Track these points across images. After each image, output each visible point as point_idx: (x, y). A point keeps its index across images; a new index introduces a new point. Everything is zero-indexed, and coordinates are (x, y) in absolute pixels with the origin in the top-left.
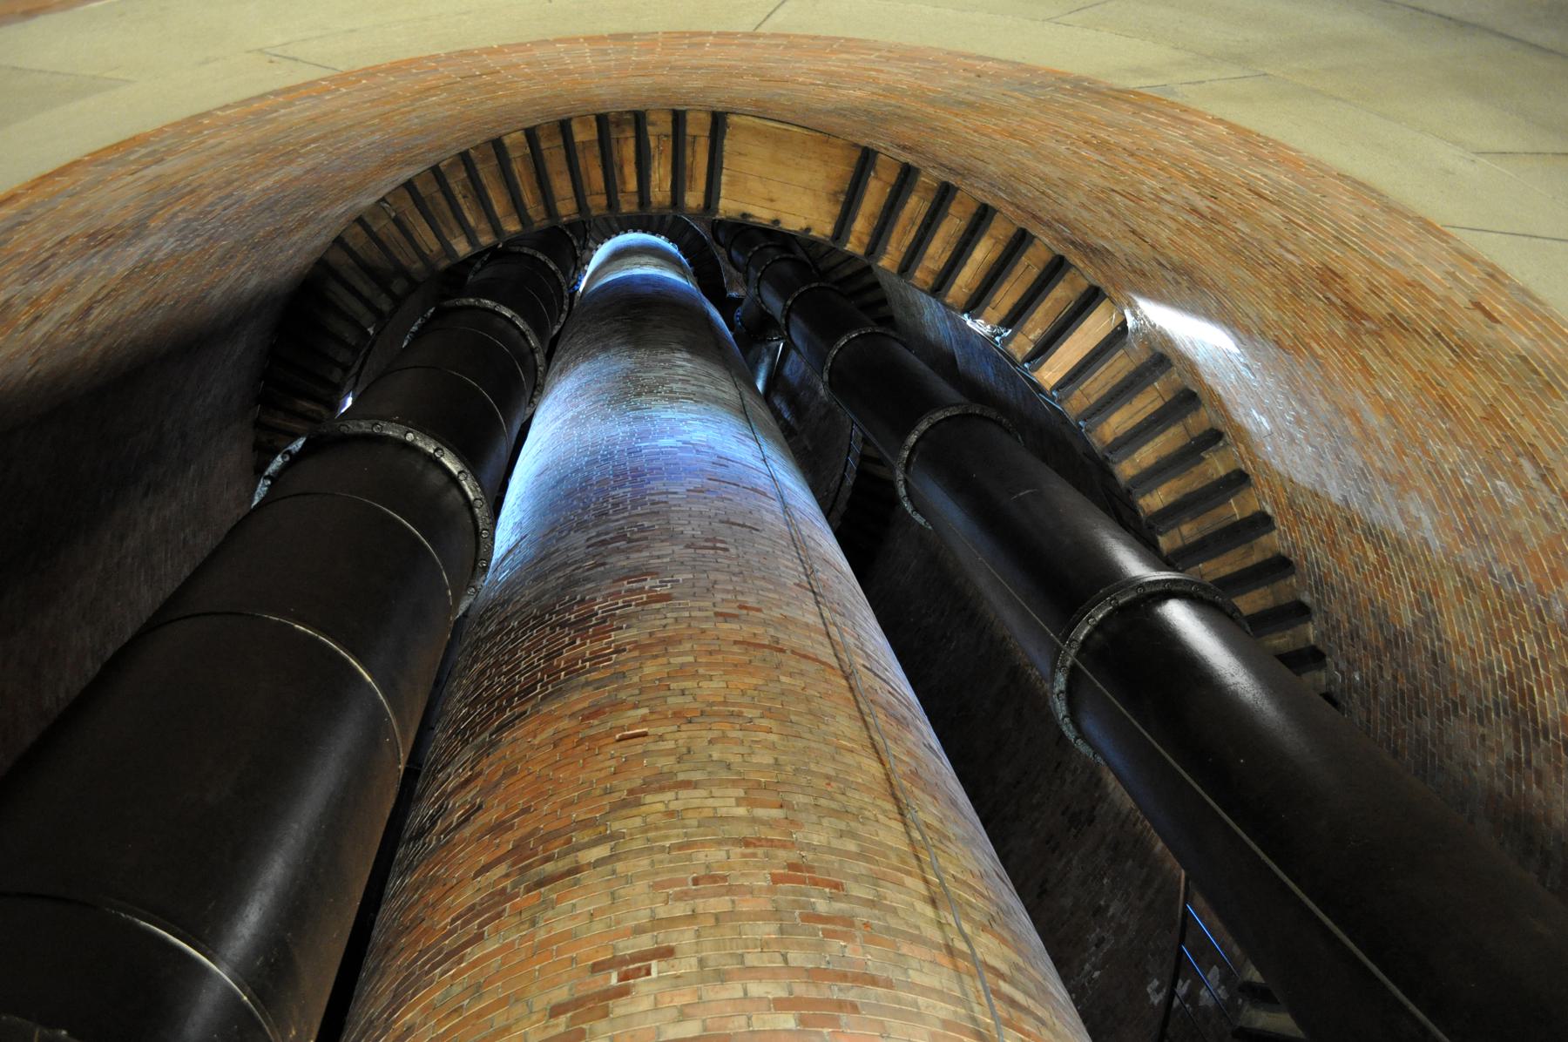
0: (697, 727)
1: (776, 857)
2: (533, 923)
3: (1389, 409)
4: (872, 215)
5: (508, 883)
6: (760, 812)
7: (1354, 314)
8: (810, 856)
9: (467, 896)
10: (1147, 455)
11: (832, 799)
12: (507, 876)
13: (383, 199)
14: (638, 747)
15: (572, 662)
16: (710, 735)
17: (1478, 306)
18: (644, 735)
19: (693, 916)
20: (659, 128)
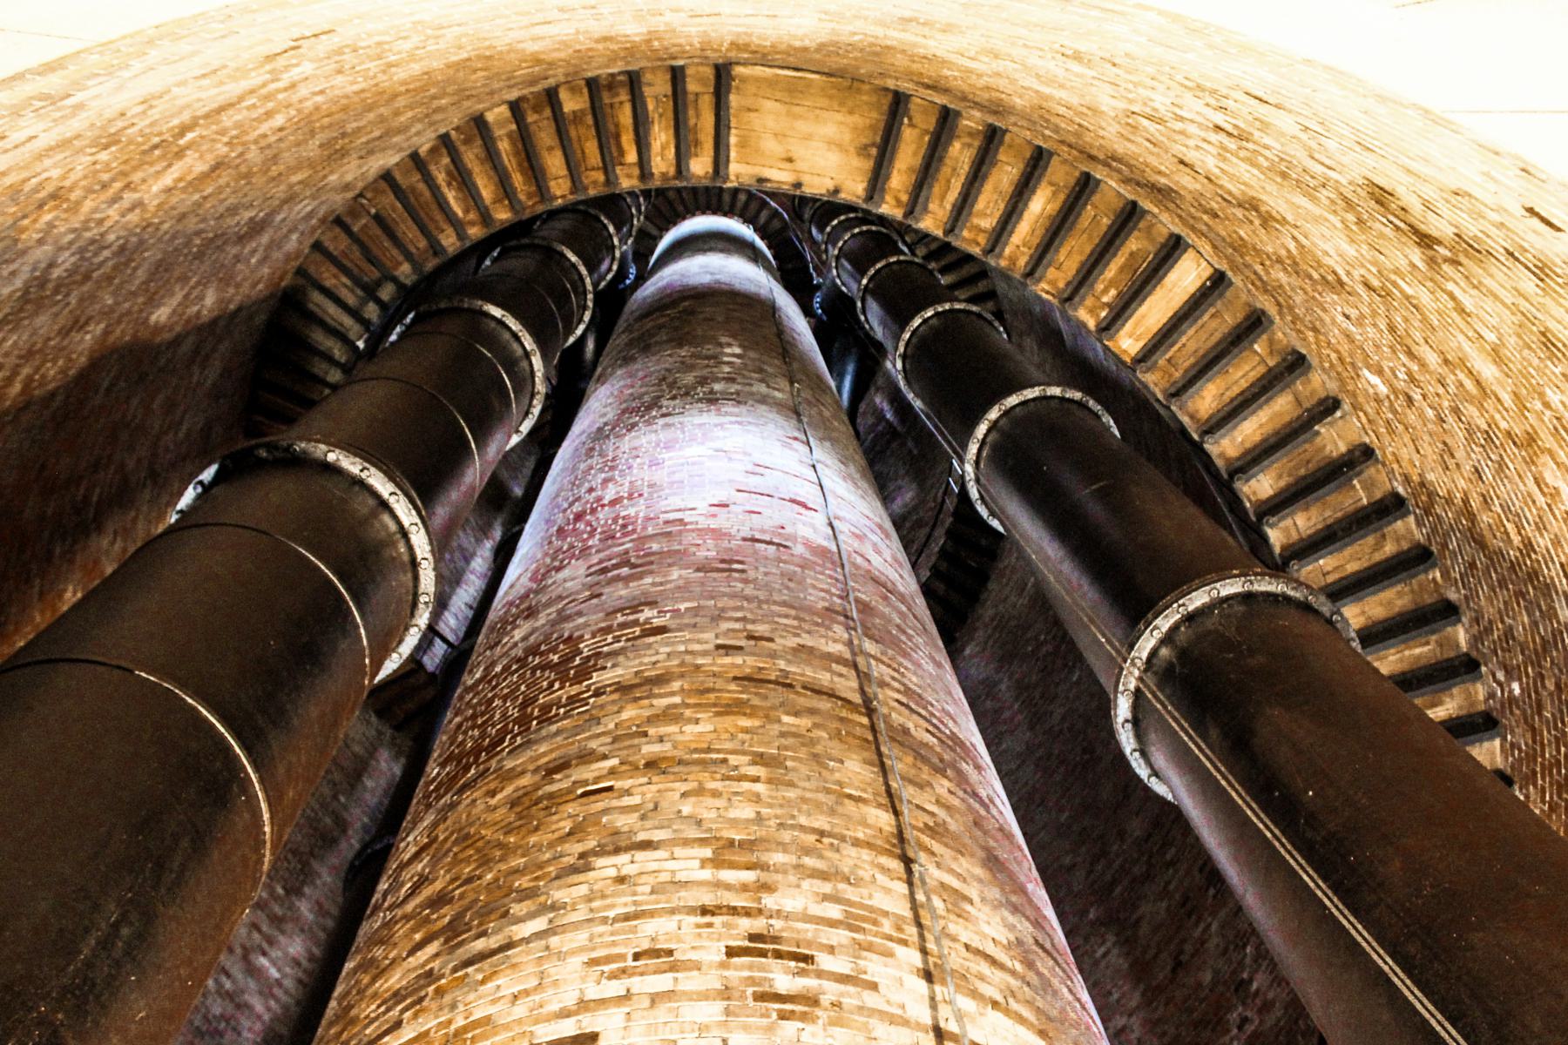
0: (672, 777)
1: (736, 926)
2: (453, 1006)
3: (1496, 355)
4: (910, 169)
5: (436, 964)
6: (728, 875)
7: (1426, 241)
8: (778, 924)
9: (395, 980)
10: (1250, 430)
11: (821, 857)
12: (437, 955)
13: (361, 195)
14: (599, 805)
15: (546, 708)
16: (684, 787)
17: (1531, 211)
18: (610, 789)
19: (627, 996)
20: (657, 89)
